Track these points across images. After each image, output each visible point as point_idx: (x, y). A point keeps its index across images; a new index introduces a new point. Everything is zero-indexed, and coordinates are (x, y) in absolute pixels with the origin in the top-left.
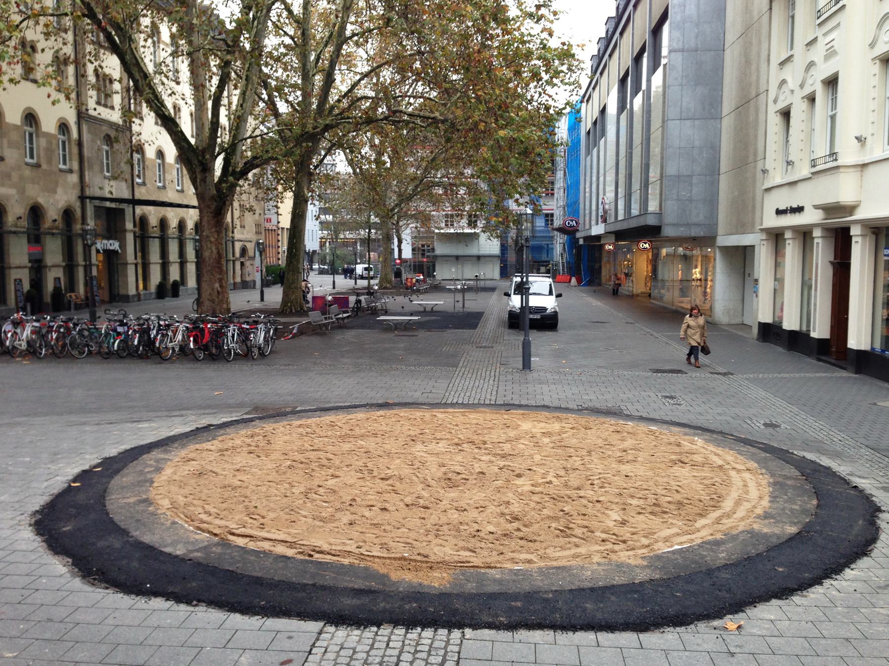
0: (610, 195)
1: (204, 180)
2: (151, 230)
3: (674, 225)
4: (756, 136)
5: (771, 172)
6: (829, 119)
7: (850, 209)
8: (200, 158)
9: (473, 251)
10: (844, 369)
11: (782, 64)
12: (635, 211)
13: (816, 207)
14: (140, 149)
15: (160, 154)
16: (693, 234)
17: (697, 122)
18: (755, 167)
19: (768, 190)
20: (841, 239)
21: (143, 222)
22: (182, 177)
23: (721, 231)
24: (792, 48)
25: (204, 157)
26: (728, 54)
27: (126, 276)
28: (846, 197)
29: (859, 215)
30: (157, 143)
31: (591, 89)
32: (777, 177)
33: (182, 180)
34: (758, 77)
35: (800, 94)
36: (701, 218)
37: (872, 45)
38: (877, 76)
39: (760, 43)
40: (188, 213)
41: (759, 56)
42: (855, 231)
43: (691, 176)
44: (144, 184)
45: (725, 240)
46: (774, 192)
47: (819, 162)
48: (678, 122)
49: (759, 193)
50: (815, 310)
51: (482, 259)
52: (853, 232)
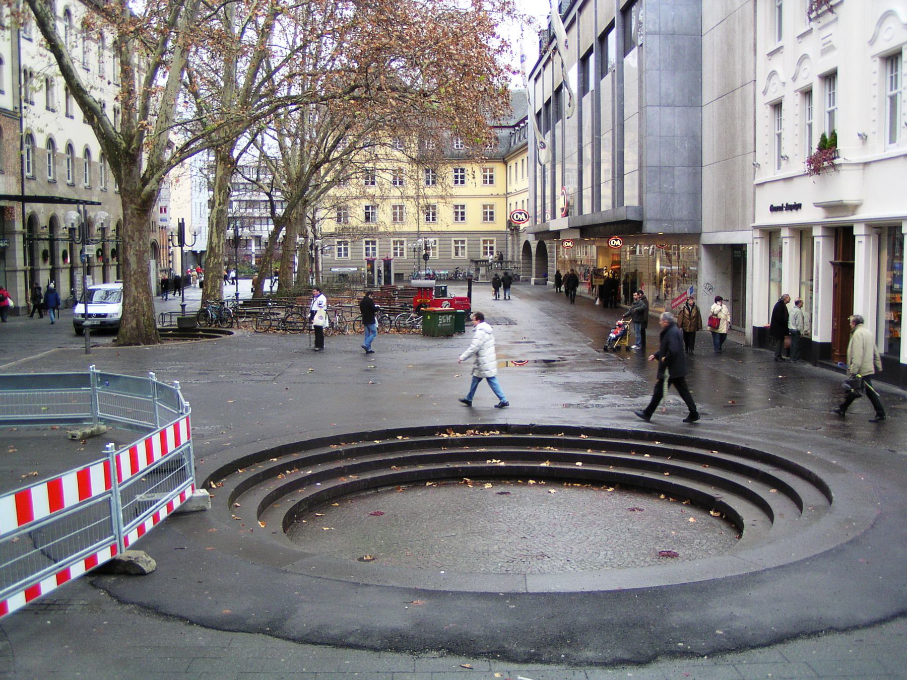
2: (39, 228)
3: (657, 220)
6: (827, 115)
7: (855, 208)
11: (771, 54)
12: (606, 203)
13: (817, 205)
14: (30, 137)
15: (87, 152)
17: (677, 110)
20: (842, 238)
21: (31, 222)
22: (105, 173)
24: (780, 39)
26: (706, 40)
27: (16, 286)
29: (864, 214)
30: (48, 131)
31: (540, 66)
33: (73, 173)
34: (743, 66)
37: (872, 42)
39: (744, 31)
42: (859, 230)
44: (33, 178)
45: (709, 238)
48: (657, 108)
49: (750, 190)
50: (817, 312)
52: (856, 232)
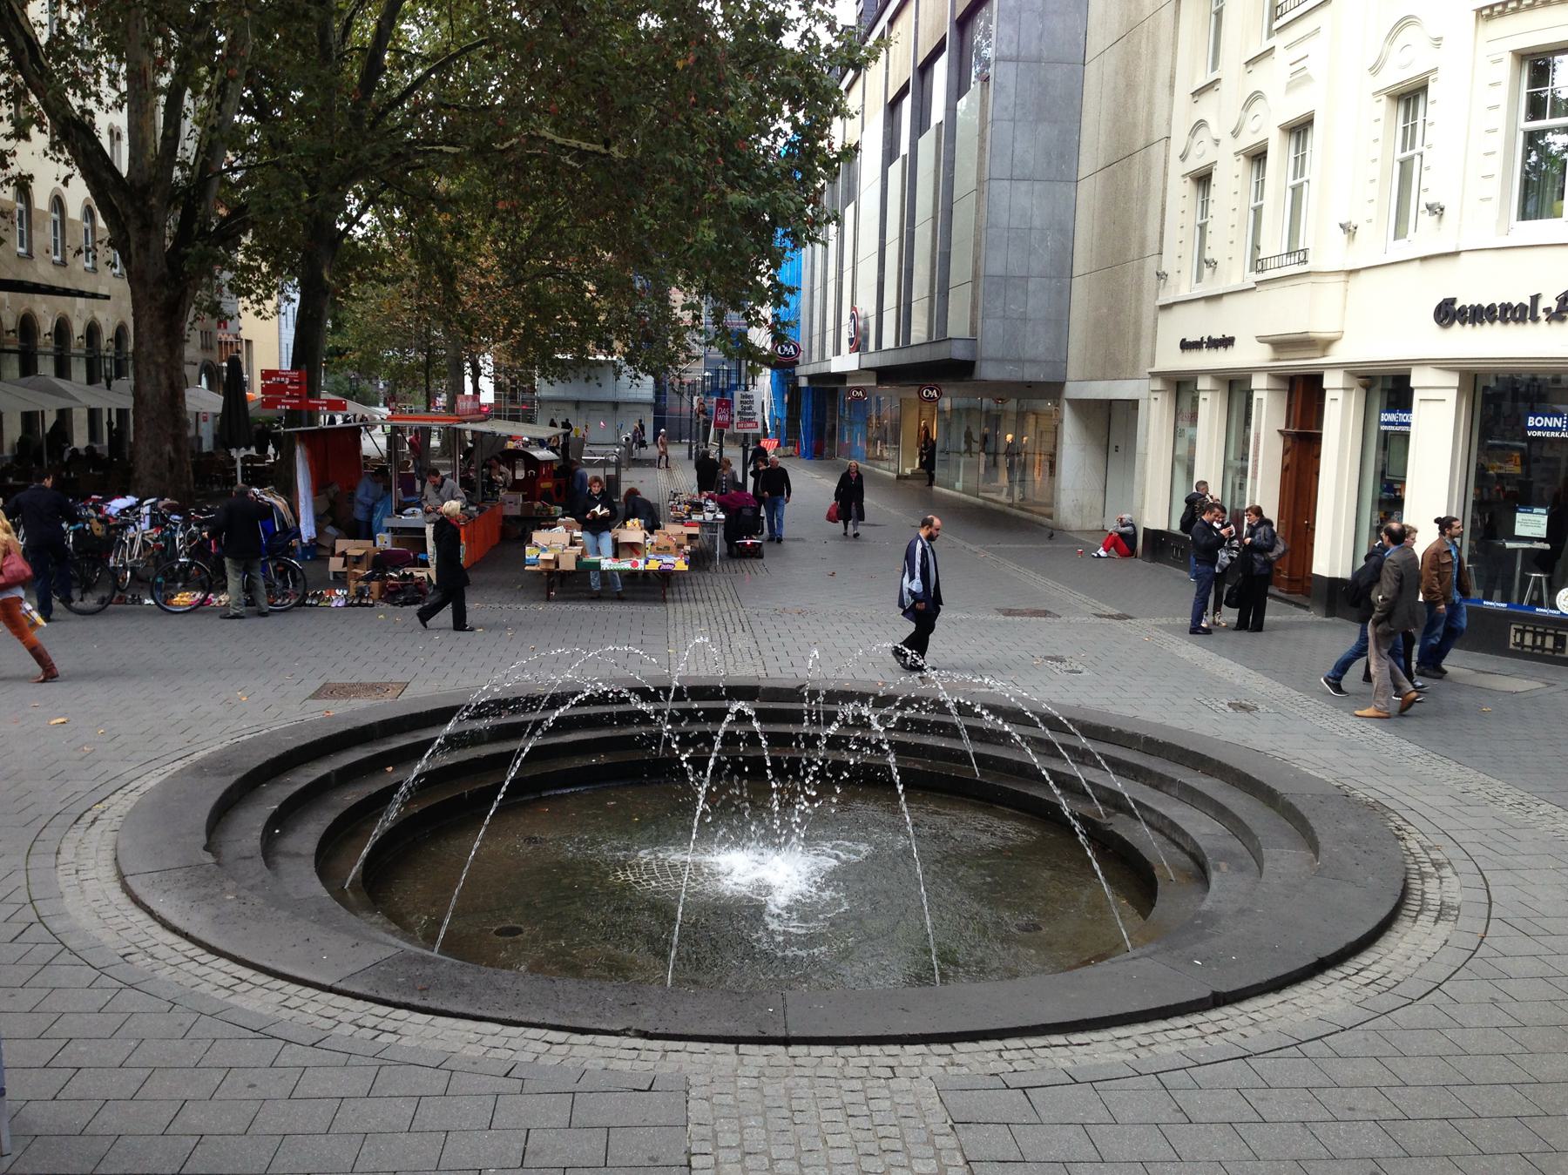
0: (867, 306)
1: (144, 246)
4: (1144, 215)
5: (1173, 278)
7: (1325, 345)
8: (138, 204)
9: (606, 393)
10: (1307, 608)
11: (1198, 93)
12: (919, 332)
13: (1262, 339)
16: (1027, 378)
17: (1037, 186)
18: (1141, 268)
19: (1166, 307)
20: (1304, 393)
23: (1072, 372)
24: (1214, 67)
25: (145, 203)
26: (1091, 71)
28: (1319, 327)
29: (1338, 354)
32: (1183, 286)
34: (1150, 114)
35: (1231, 146)
36: (1040, 351)
37: (1375, 69)
38: (1381, 123)
40: (73, 306)
41: (1153, 80)
42: (1332, 381)
43: (1026, 278)
46: (1176, 309)
47: (1270, 264)
48: (1007, 183)
51: (622, 409)
